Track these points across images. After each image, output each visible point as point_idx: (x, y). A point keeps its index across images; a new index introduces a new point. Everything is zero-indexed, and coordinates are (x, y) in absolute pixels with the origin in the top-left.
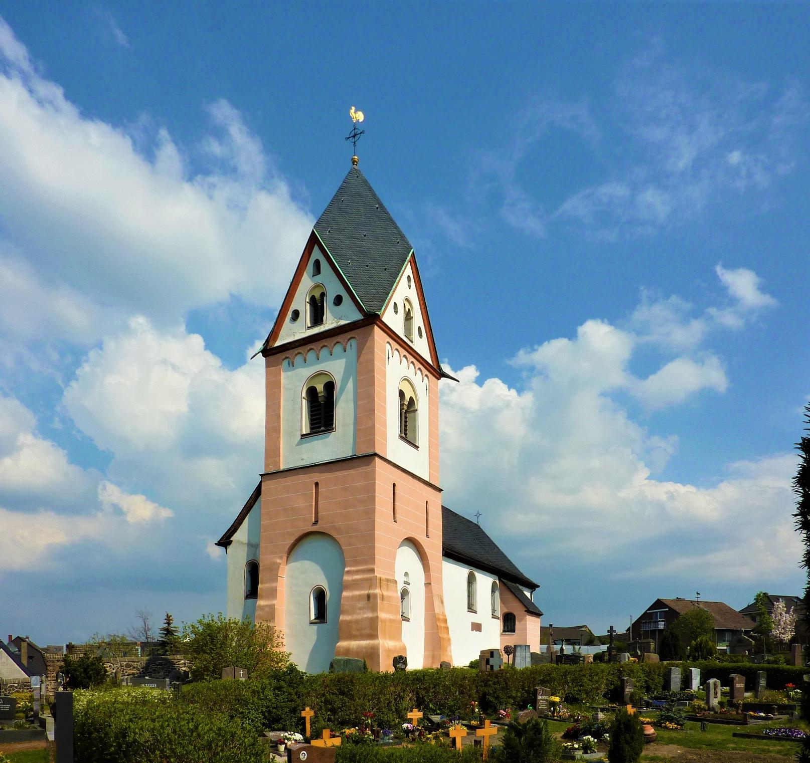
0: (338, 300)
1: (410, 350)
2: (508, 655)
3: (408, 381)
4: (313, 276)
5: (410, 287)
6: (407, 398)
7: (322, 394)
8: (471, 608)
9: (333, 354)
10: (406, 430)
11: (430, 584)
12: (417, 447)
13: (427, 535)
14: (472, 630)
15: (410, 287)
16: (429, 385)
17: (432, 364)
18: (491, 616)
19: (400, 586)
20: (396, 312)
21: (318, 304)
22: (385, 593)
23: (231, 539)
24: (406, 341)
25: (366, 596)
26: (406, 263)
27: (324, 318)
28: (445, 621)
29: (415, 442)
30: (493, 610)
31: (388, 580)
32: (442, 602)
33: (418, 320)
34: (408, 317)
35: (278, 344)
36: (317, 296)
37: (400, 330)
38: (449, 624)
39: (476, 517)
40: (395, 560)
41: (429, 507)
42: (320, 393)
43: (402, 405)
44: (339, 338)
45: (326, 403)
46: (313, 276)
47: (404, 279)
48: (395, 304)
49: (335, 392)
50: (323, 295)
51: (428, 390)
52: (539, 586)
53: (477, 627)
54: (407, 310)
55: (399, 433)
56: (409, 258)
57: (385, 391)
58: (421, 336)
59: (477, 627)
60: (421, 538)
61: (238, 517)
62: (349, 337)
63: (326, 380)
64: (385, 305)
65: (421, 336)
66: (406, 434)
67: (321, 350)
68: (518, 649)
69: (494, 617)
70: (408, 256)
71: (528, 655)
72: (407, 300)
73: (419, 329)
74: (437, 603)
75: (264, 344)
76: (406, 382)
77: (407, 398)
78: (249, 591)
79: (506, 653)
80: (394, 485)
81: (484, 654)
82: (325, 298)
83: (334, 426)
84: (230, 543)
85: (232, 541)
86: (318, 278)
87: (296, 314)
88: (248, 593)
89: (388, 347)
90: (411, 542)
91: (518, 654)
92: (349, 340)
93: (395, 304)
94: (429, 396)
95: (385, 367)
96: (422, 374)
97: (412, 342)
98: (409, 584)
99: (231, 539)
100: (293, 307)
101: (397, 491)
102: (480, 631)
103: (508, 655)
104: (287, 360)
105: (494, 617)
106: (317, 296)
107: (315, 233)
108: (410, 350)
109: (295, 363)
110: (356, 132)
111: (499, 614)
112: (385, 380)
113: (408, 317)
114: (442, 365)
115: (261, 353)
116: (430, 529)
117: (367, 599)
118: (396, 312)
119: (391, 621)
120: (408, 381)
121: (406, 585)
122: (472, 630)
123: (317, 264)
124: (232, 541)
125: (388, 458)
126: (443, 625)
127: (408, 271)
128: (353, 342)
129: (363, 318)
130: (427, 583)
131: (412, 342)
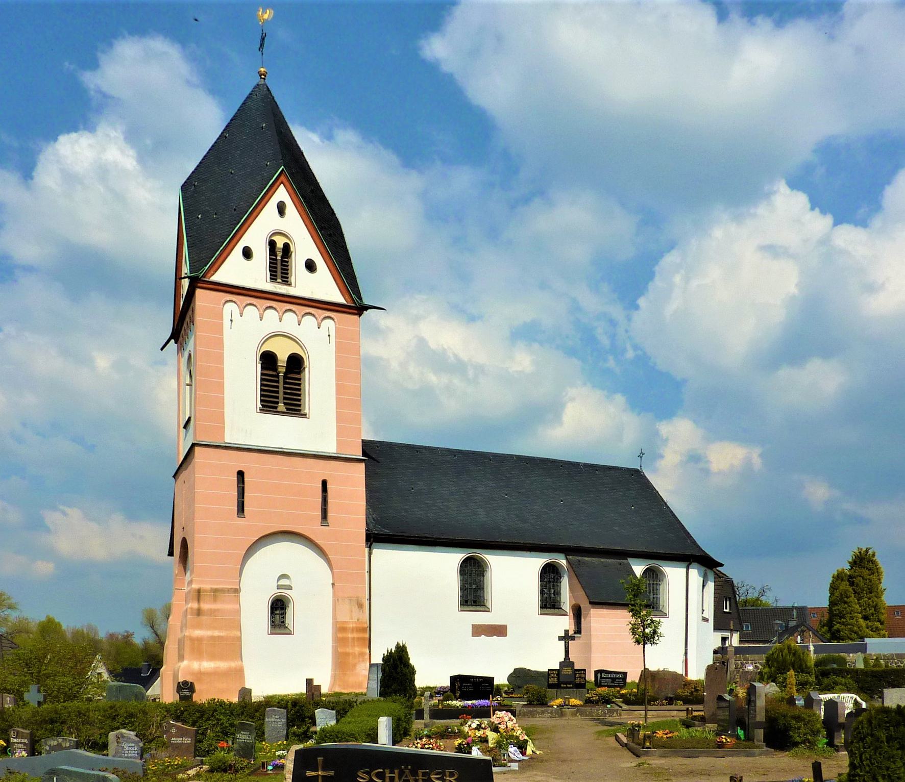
6: (282, 358)
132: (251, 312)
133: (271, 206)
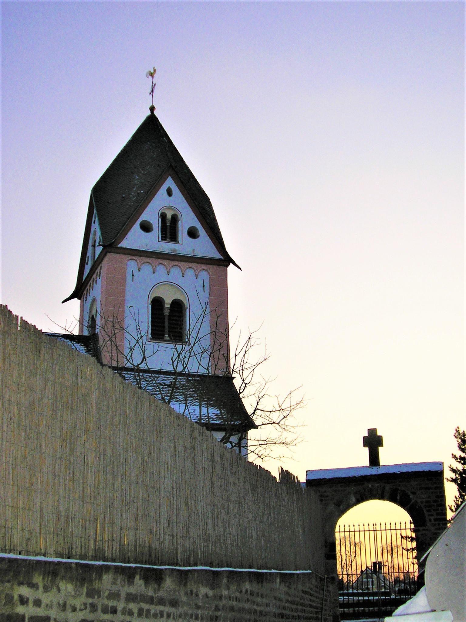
132: (147, 269)
133: (162, 191)
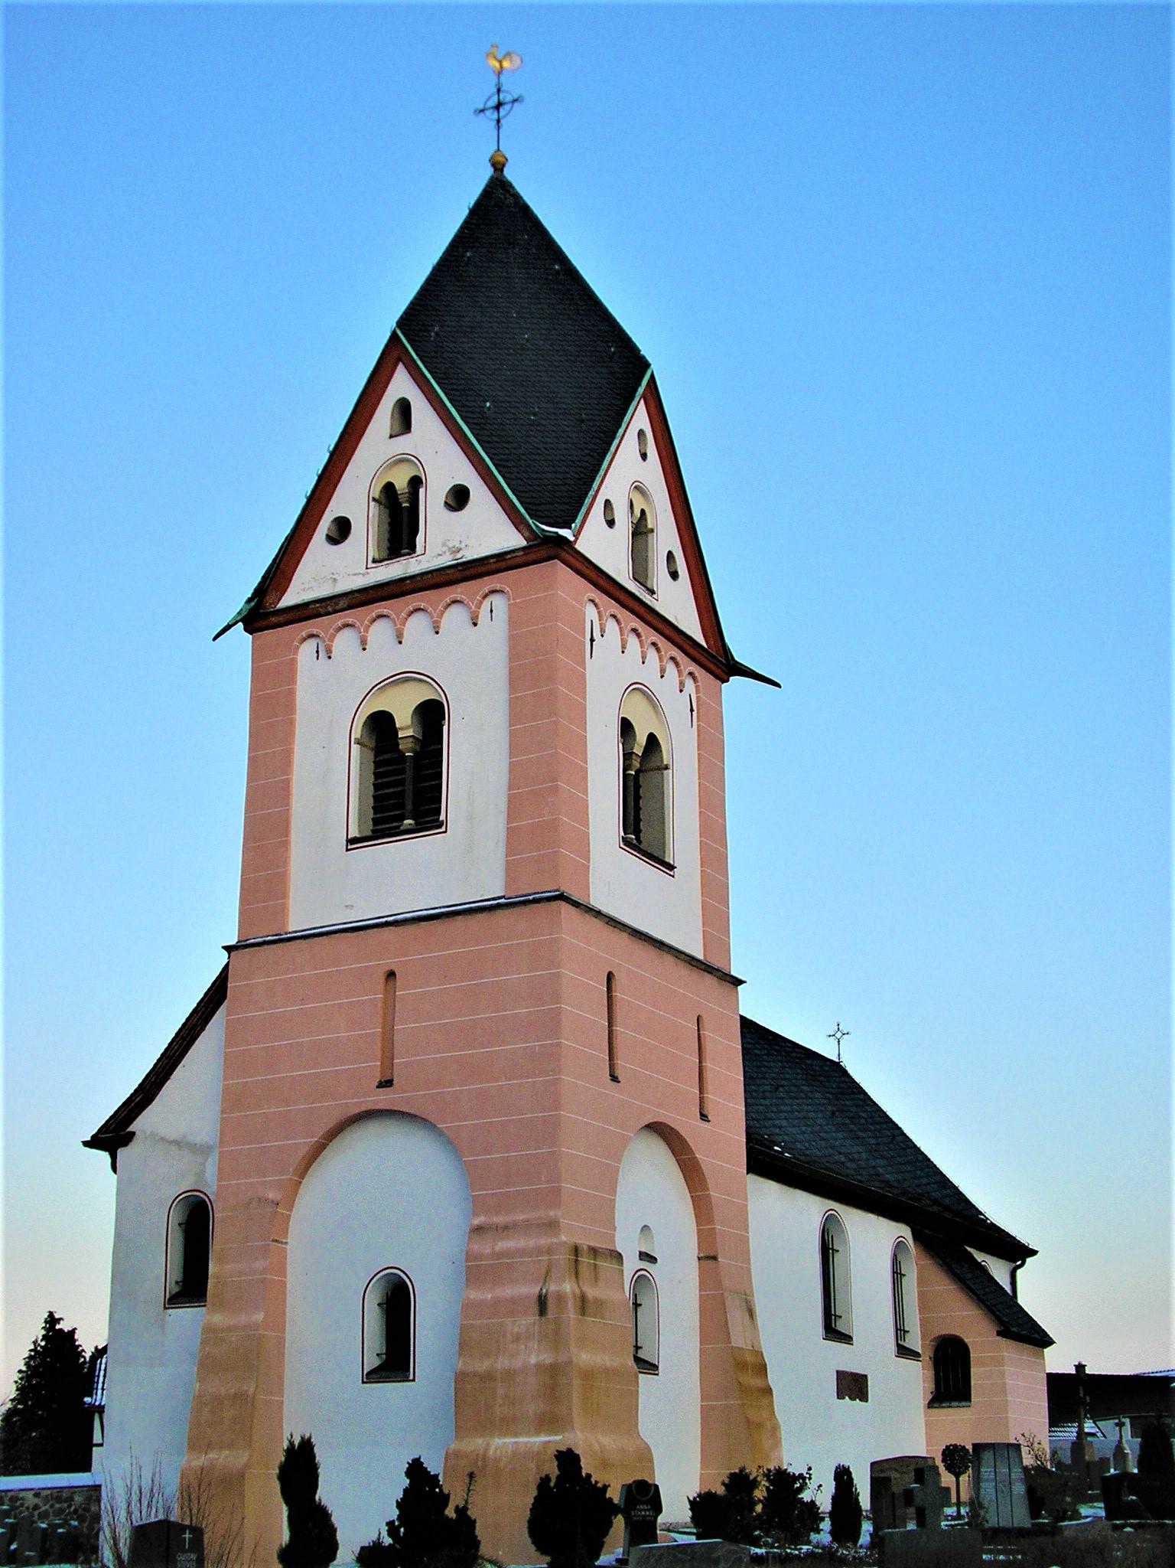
0: (459, 498)
1: (649, 617)
2: (957, 1476)
3: (643, 693)
4: (391, 437)
5: (644, 456)
7: (410, 733)
8: (834, 1332)
9: (441, 631)
10: (637, 820)
11: (715, 1258)
12: (671, 867)
13: (702, 1114)
14: (840, 1395)
15: (644, 456)
16: (698, 698)
17: (706, 646)
18: (892, 1348)
19: (631, 1264)
20: (611, 523)
21: (400, 504)
22: (591, 1292)
23: (131, 1129)
24: (637, 593)
25: (535, 1299)
26: (634, 403)
27: (419, 540)
28: (762, 1369)
29: (664, 857)
30: (900, 1331)
31: (594, 1251)
32: (751, 1313)
33: (666, 538)
34: (640, 531)
35: (288, 600)
36: (401, 483)
37: (619, 568)
38: (773, 1378)
39: (833, 1041)
40: (614, 1192)
41: (706, 1033)
42: (402, 729)
43: (628, 756)
44: (459, 590)
45: (417, 756)
46: (391, 437)
47: (631, 439)
48: (608, 503)
49: (445, 728)
50: (416, 483)
51: (694, 713)
52: (1034, 1253)
53: (853, 1386)
54: (637, 513)
55: (622, 834)
56: (641, 390)
57: (583, 724)
58: (674, 575)
59: (853, 1386)
60: (686, 1124)
61: (156, 1065)
62: (486, 590)
63: (423, 694)
64: (583, 510)
65: (674, 575)
66: (637, 832)
67: (409, 619)
68: (987, 1456)
69: (903, 1351)
70: (640, 385)
71: (1017, 1474)
72: (638, 488)
73: (670, 556)
74: (736, 1316)
75: (249, 601)
76: (638, 696)
77: (641, 739)
78: (177, 1283)
79: (948, 1468)
80: (610, 977)
81: (882, 1471)
82: (422, 491)
83: (442, 817)
84: (128, 1139)
85: (133, 1134)
86: (404, 444)
87: (342, 529)
88: (176, 1289)
89: (591, 612)
90: (660, 1130)
91: (986, 1471)
92: (485, 596)
93: (608, 503)
94: (698, 726)
95: (583, 664)
96: (680, 672)
97: (652, 592)
98: (652, 1259)
99: (131, 1129)
100: (335, 509)
101: (617, 994)
102: (840, 1375)
103: (957, 1476)
104: (312, 643)
105: (903, 1351)
106: (401, 483)
107: (397, 335)
108: (649, 617)
109: (333, 649)
110: (501, 98)
111: (915, 1341)
112: (584, 698)
113: (640, 531)
114: (639, 516)
115: (240, 624)
116: (710, 1096)
117: (536, 1309)
118: (611, 523)
119: (608, 1372)
120: (643, 693)
121: (645, 1265)
122: (840, 1395)
123: (404, 409)
124: (133, 1134)
125: (596, 902)
126: (757, 1382)
127: (639, 418)
128: (498, 601)
129: (524, 543)
130: (708, 1258)
131: (652, 592)
